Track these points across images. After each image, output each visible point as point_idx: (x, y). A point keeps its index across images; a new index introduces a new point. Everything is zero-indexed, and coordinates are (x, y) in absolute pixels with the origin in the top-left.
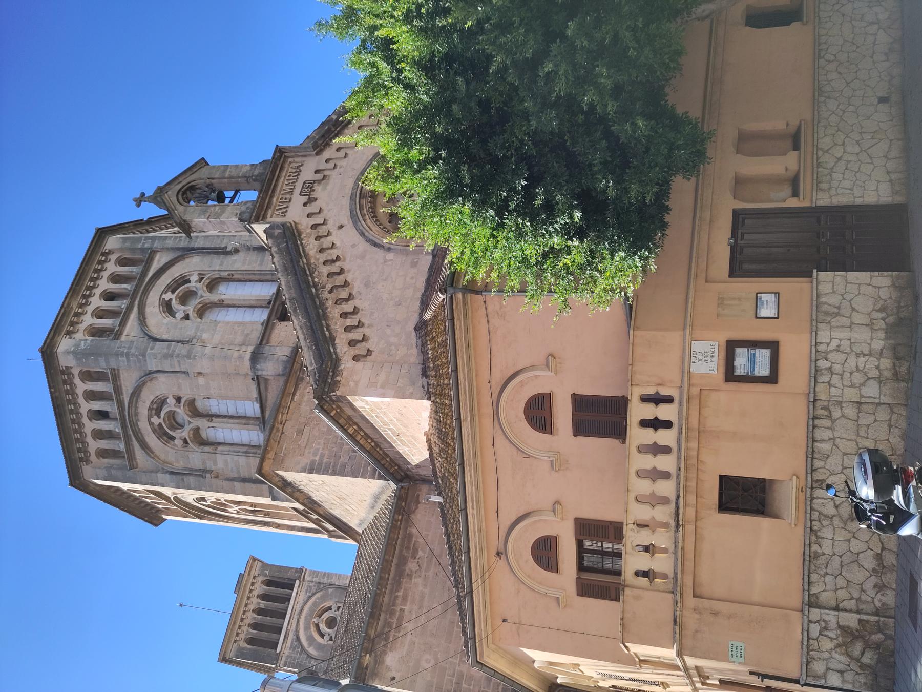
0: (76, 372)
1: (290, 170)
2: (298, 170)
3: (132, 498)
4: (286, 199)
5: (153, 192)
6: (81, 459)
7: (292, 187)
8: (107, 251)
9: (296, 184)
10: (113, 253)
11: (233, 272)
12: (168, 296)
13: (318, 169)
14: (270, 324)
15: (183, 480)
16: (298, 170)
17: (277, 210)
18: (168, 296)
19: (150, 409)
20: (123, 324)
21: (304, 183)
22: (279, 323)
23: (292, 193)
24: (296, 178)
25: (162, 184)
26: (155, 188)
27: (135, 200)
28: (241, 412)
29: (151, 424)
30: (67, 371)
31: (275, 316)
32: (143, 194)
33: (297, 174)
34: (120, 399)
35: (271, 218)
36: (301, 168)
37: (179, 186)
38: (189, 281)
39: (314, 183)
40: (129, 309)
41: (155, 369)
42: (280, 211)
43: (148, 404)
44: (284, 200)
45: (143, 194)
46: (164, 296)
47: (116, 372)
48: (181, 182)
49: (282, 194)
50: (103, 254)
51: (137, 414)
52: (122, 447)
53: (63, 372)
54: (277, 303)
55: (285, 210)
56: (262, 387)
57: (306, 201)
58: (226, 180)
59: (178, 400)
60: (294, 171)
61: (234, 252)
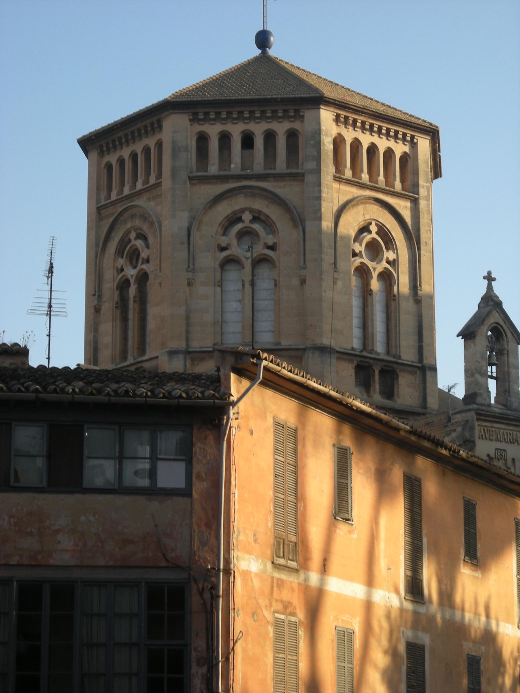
0: (296, 125)
1: (515, 433)
2: (514, 441)
3: (420, 543)
4: (492, 435)
5: (495, 292)
6: (196, 114)
7: (501, 440)
8: (415, 140)
9: (504, 443)
10: (413, 147)
11: (397, 300)
12: (374, 228)
13: (516, 461)
14: (352, 358)
15: (182, 243)
16: (514, 441)
17: (484, 430)
18: (374, 228)
19: (260, 212)
20: (348, 182)
21: (505, 450)
22: (354, 366)
23: (497, 440)
24: (509, 441)
25: (505, 306)
26: (501, 298)
27: (489, 273)
28: (259, 316)
29: (243, 211)
30: (298, 116)
31: (361, 361)
32: (494, 279)
33: (511, 440)
34: (270, 177)
35: (478, 425)
36: (516, 444)
37: (502, 323)
38: (388, 249)
39: (504, 459)
40: (362, 186)
41: (307, 229)
42: (483, 434)
43: (265, 210)
44: (491, 433)
45: (494, 279)
46: (374, 223)
47: (300, 178)
48: (505, 324)
49: (496, 431)
50: (412, 137)
51: (253, 195)
52: (213, 169)
53: (297, 111)
54: (371, 361)
55: (484, 437)
56: (293, 353)
57: (491, 456)
58: (506, 370)
59: (272, 248)
60: (514, 438)
61: (417, 299)
